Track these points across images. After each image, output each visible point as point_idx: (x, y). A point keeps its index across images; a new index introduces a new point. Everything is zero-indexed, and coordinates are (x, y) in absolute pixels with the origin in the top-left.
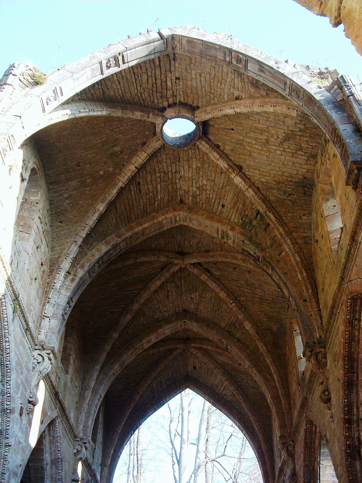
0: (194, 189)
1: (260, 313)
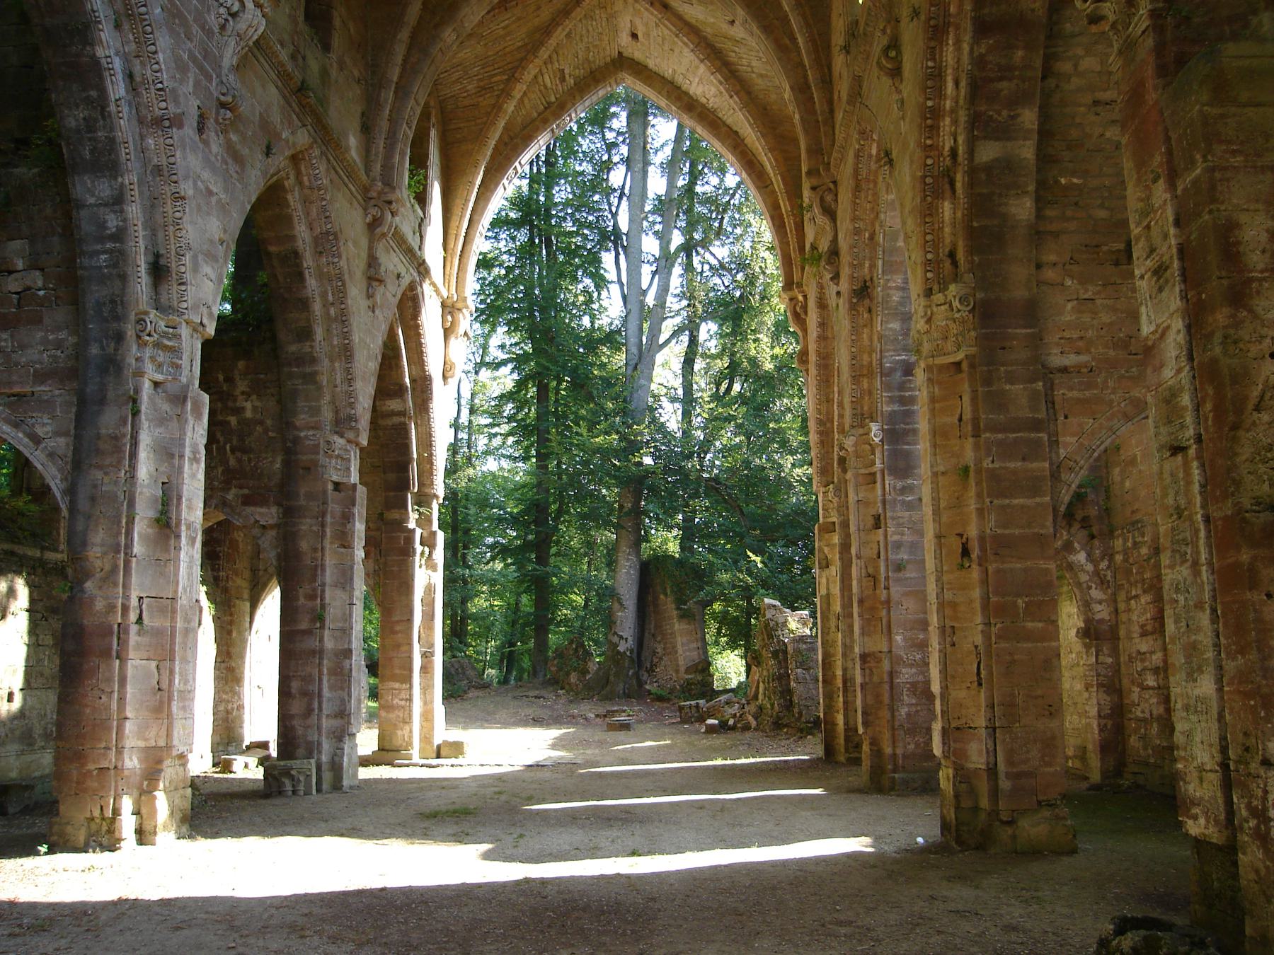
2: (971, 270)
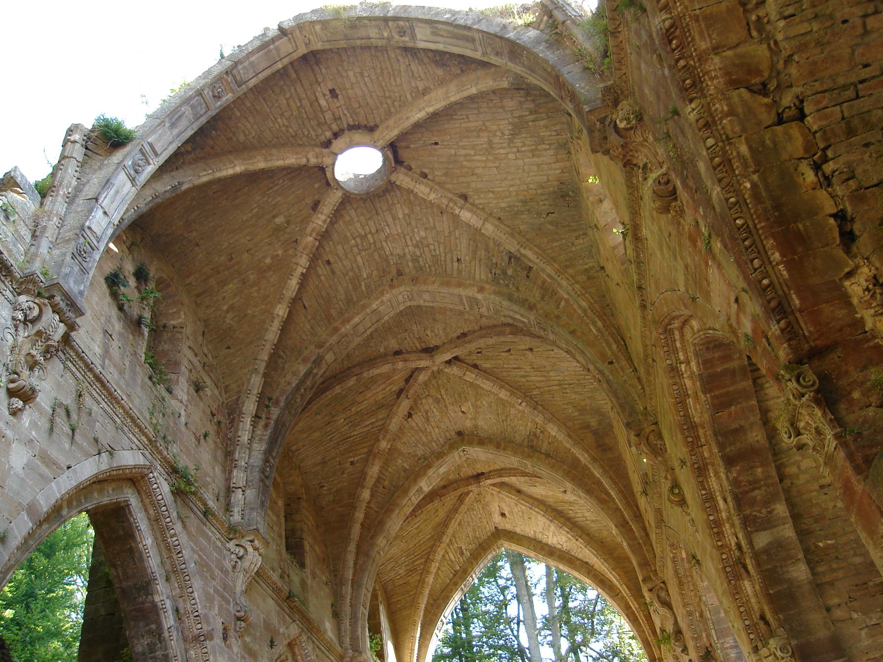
0: (411, 248)
1: (565, 406)
2: (781, 626)
